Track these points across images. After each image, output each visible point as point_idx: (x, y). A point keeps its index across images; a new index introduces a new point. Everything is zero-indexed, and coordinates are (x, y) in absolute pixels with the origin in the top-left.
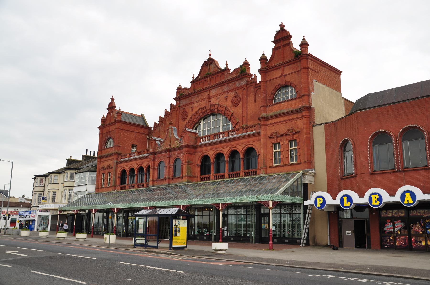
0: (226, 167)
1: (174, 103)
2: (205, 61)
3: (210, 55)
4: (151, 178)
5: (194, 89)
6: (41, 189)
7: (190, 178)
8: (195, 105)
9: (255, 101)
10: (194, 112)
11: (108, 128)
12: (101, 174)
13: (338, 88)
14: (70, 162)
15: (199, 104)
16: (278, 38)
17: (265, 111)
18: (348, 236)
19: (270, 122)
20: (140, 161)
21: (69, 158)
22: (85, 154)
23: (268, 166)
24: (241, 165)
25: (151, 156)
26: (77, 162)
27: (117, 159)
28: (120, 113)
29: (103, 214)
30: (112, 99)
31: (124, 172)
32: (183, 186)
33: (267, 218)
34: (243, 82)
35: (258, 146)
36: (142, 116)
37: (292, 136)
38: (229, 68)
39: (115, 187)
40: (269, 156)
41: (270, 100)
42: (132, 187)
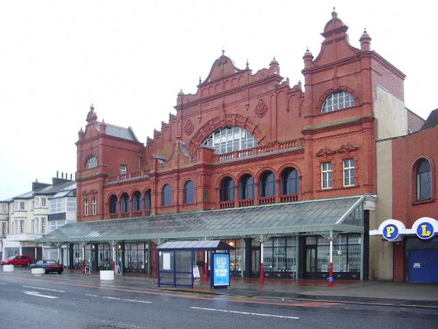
0: (252, 190)
1: (175, 113)
2: (217, 60)
3: (223, 51)
4: (153, 205)
5: (202, 94)
7: (207, 204)
8: (204, 115)
9: (288, 110)
10: (202, 124)
12: (82, 200)
13: (402, 99)
14: (37, 187)
15: (210, 113)
16: (329, 30)
17: (311, 123)
18: (417, 269)
19: (318, 136)
20: (135, 184)
21: (35, 181)
22: (56, 177)
23: (314, 190)
24: (273, 187)
26: (45, 186)
27: (104, 181)
28: (104, 126)
29: (92, 247)
30: (92, 108)
31: (113, 198)
32: (174, 217)
33: (258, 252)
34: (271, 87)
35: (302, 166)
36: (130, 131)
37: (348, 153)
38: (250, 68)
39: (103, 216)
40: (316, 178)
41: (317, 112)
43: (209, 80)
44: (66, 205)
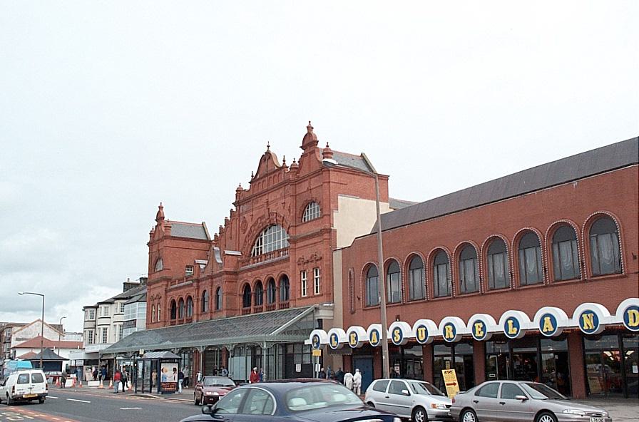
3: (268, 146)
4: (195, 312)
6: (91, 324)
8: (255, 212)
11: (307, 183)
14: (127, 286)
15: (257, 212)
16: (306, 143)
25: (195, 284)
28: (168, 228)
30: (310, 128)
31: (173, 302)
42: (271, 308)
43: (258, 177)
44: (139, 311)
